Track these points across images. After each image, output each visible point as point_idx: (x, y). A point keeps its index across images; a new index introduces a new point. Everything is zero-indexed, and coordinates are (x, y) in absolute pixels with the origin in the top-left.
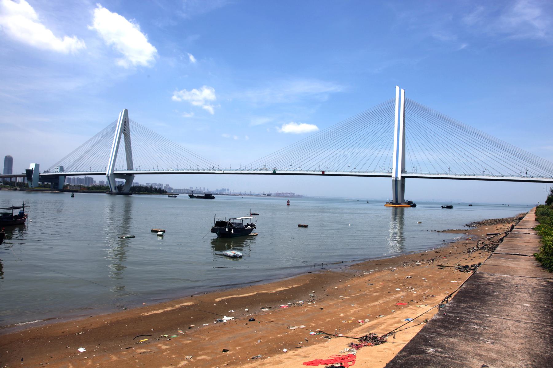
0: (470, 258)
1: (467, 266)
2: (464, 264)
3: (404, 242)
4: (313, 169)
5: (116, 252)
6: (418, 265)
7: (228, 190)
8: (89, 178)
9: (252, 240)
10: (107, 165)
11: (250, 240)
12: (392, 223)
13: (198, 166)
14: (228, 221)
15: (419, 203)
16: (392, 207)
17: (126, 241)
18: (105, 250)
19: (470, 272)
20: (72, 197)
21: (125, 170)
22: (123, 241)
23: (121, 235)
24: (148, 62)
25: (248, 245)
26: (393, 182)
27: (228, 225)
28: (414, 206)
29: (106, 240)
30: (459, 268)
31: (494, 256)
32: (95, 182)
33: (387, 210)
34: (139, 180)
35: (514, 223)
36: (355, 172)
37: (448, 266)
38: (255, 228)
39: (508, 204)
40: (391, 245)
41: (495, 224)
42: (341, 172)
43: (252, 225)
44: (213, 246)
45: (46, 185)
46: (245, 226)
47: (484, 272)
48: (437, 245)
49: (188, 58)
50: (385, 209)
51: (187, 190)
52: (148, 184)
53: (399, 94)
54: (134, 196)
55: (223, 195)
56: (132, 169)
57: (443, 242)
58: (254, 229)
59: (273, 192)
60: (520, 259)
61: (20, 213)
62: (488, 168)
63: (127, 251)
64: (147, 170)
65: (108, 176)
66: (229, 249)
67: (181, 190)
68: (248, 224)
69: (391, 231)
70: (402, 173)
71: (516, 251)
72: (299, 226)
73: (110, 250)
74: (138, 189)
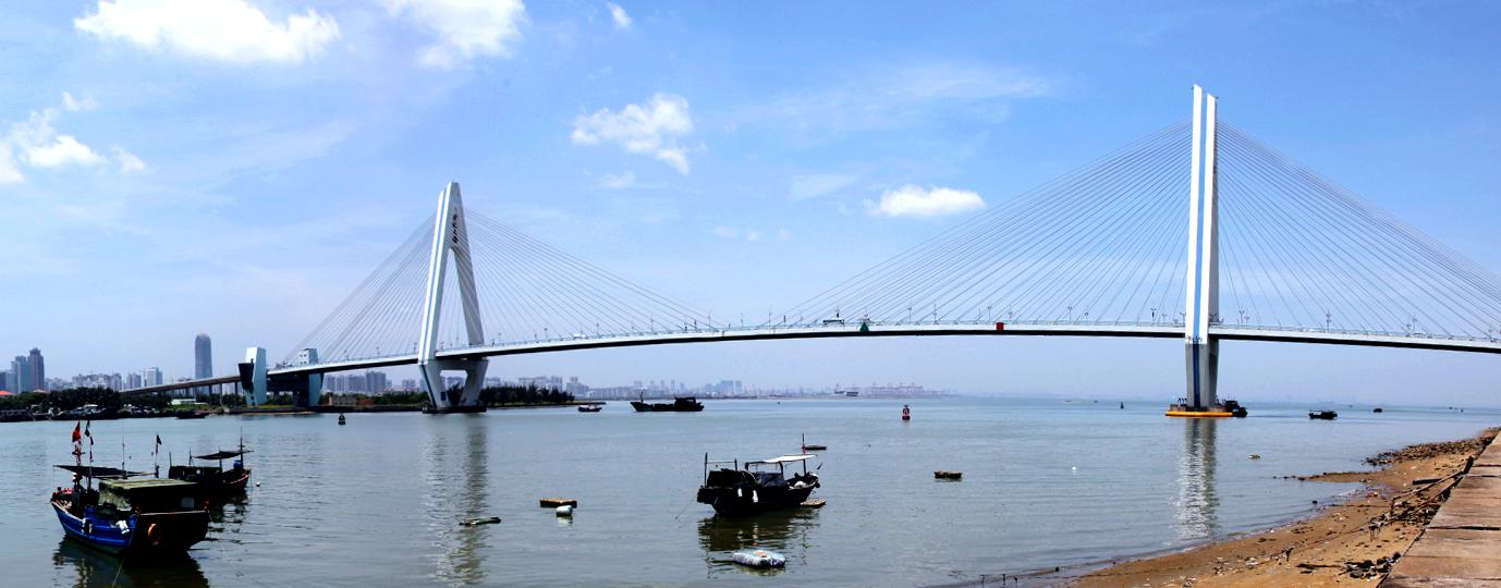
0: (1375, 543)
1: (1368, 564)
2: (1361, 559)
3: (1215, 508)
4: (972, 316)
5: (458, 561)
6: (1252, 568)
7: (739, 384)
8: (375, 375)
9: (809, 518)
10: (419, 337)
11: (805, 518)
12: (1184, 460)
13: (652, 321)
14: (741, 468)
15: (1255, 406)
16: (1184, 419)
17: (478, 532)
18: (429, 556)
19: (1375, 578)
20: (340, 423)
21: (464, 347)
22: (472, 532)
23: (465, 518)
24: (505, 41)
25: (799, 532)
26: (1187, 349)
27: (744, 480)
28: (1242, 413)
29: (431, 532)
30: (1350, 570)
31: (1431, 534)
32: (390, 383)
33: (1173, 425)
34: (499, 372)
35: (1472, 454)
36: (1087, 323)
37: (1325, 566)
38: (818, 486)
39: (1462, 406)
40: (1183, 517)
41: (1432, 456)
42: (1048, 323)
43: (808, 478)
44: (705, 538)
45: (282, 397)
46: (789, 481)
47: (1404, 575)
48: (1297, 514)
49: (608, 15)
50: (1167, 425)
51: (626, 389)
52: (525, 379)
53: (1203, 109)
54: (490, 413)
55: (726, 398)
56: (481, 343)
57: (1312, 506)
58: (815, 489)
59: (862, 385)
60: (1486, 538)
61: (235, 465)
62: (1419, 316)
63: (484, 558)
64: (520, 343)
65: (423, 366)
66: (750, 544)
67: (604, 390)
68: (796, 475)
69: (1184, 482)
70: (1209, 325)
71: (1476, 520)
72: (938, 476)
73: (441, 559)
74: (499, 394)
